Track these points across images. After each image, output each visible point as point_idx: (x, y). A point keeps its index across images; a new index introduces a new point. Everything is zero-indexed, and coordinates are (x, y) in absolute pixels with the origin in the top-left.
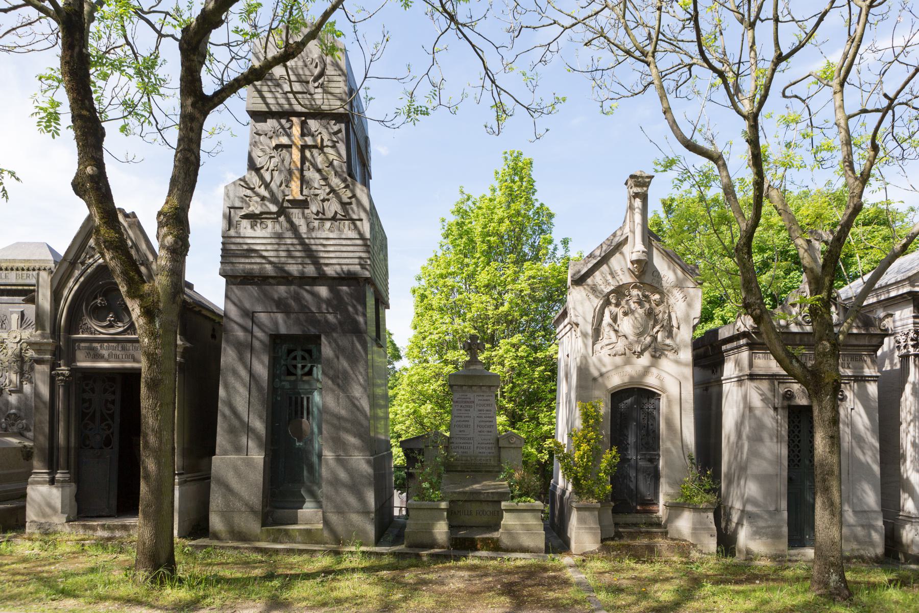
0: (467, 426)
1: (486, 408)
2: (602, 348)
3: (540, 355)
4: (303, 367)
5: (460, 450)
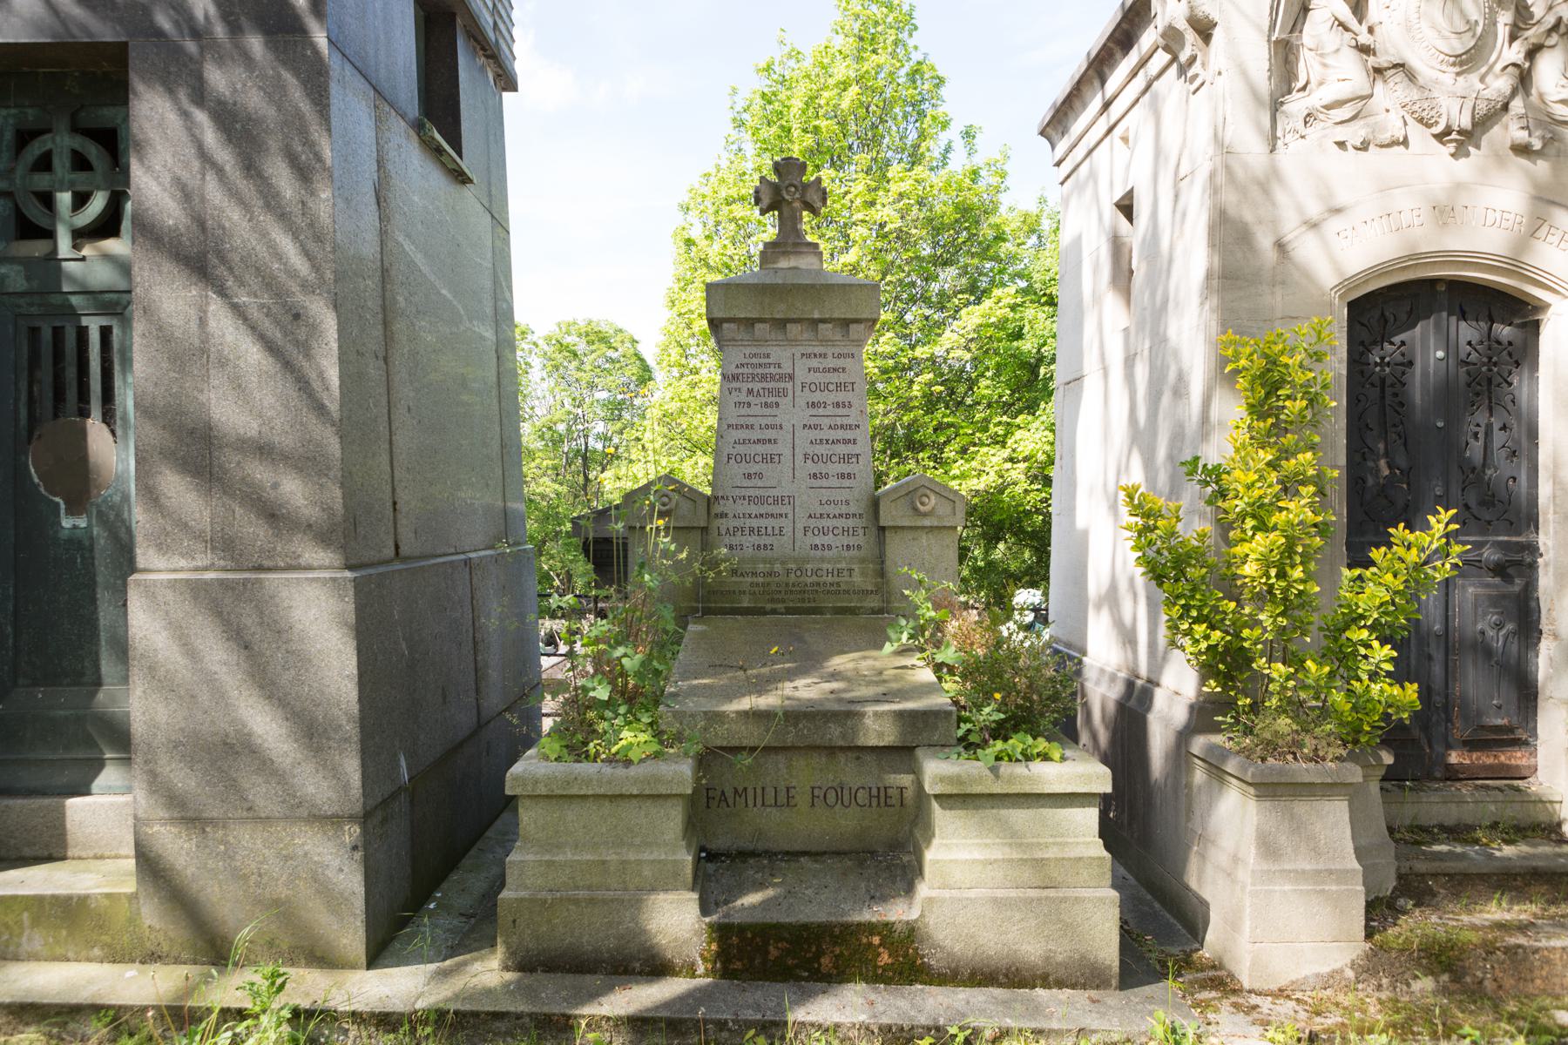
0: (769, 459)
1: (831, 397)
2: (1309, 118)
3: (921, 352)
4: (81, 200)
5: (749, 541)
